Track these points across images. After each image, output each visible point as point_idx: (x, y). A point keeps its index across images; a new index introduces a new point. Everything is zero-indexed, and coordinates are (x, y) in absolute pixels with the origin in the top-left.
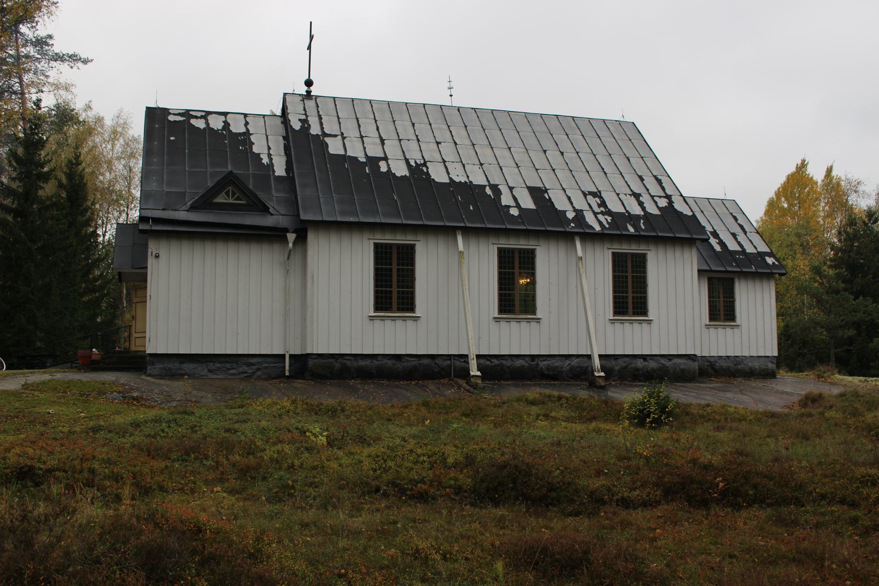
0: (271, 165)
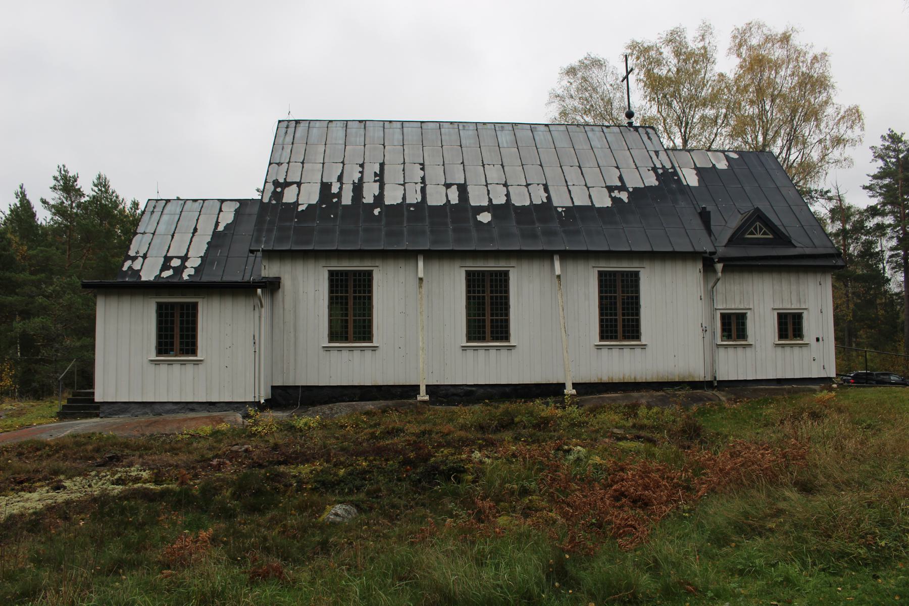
0: (339, 195)
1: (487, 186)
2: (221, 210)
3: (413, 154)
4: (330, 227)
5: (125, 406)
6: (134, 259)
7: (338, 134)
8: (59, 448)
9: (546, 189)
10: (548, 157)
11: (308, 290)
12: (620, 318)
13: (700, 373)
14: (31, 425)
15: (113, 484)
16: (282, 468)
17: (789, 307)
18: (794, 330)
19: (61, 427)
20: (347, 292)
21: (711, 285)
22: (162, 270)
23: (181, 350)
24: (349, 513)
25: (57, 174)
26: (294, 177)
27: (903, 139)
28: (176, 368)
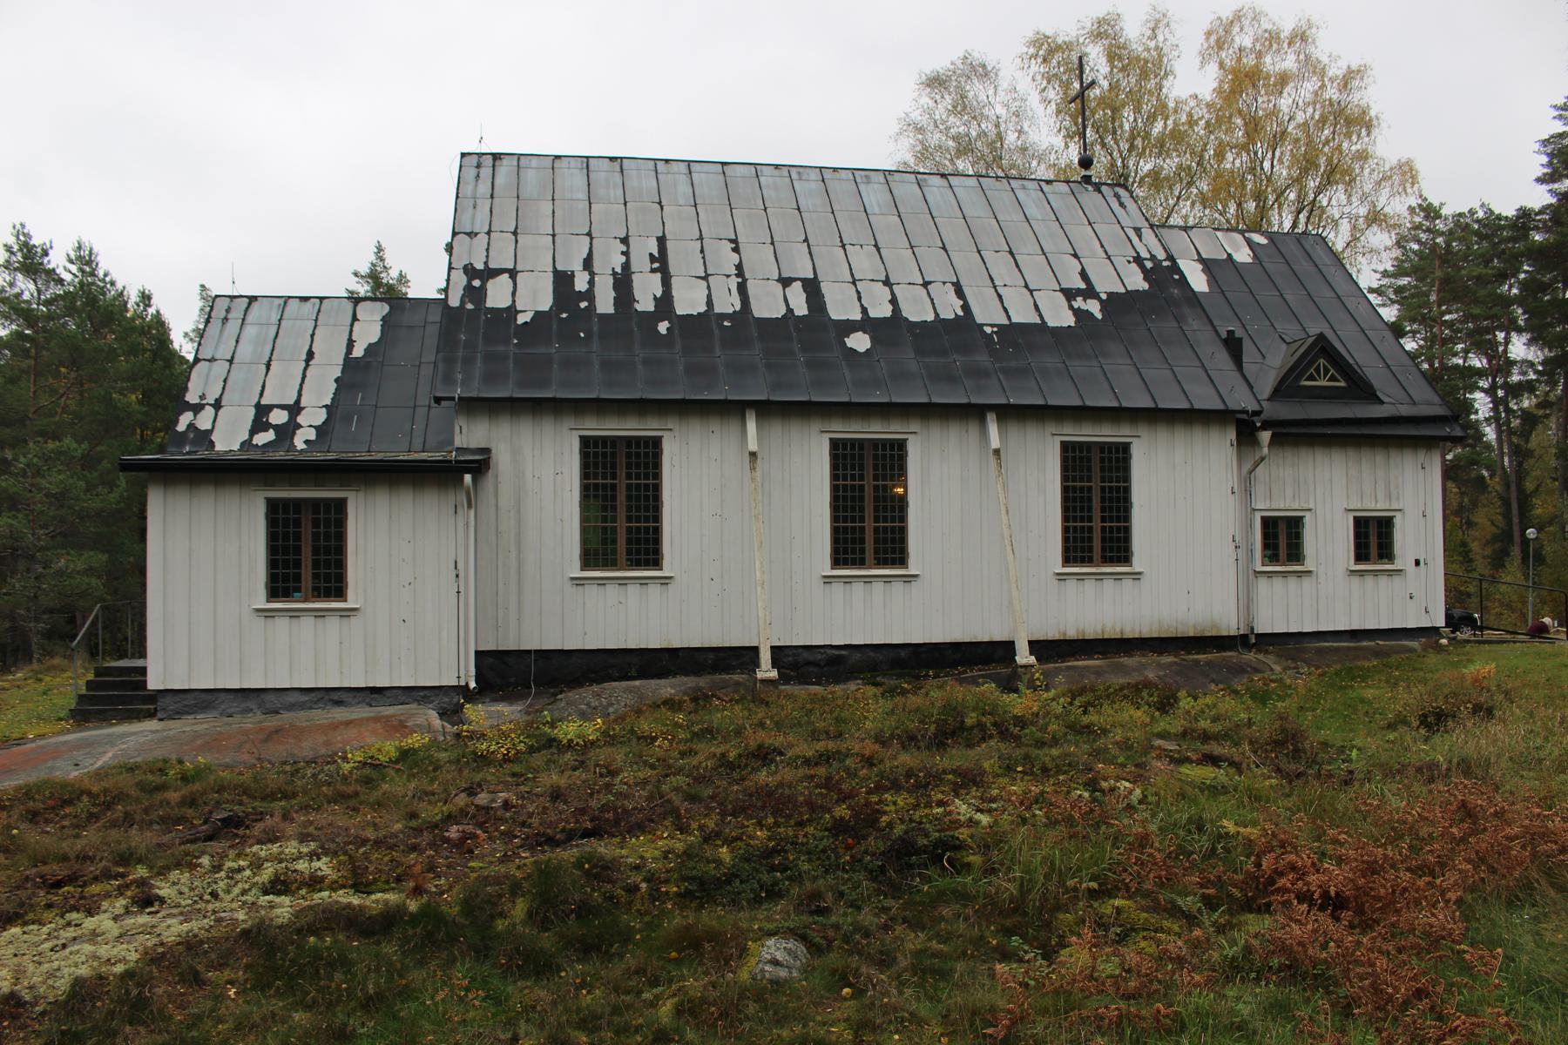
0: (589, 295)
1: (854, 283)
2: (355, 318)
3: (716, 223)
4: (564, 351)
5: (208, 697)
6: (197, 409)
7: (573, 181)
8: (103, 801)
9: (960, 293)
10: (954, 233)
11: (541, 472)
12: (1097, 524)
13: (1230, 624)
14: (22, 740)
15: (266, 893)
16: (604, 848)
17: (1372, 506)
18: (1380, 546)
19: (88, 744)
20: (614, 477)
21: (1247, 467)
22: (253, 432)
23: (315, 589)
24: (796, 957)
25: (12, 241)
26: (501, 260)
27: (1443, 212)
28: (307, 622)
